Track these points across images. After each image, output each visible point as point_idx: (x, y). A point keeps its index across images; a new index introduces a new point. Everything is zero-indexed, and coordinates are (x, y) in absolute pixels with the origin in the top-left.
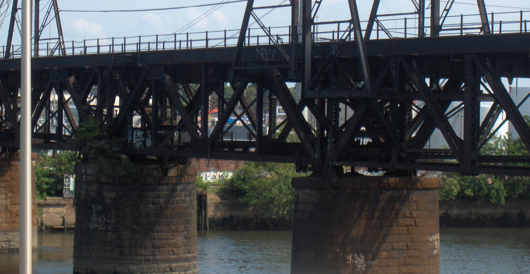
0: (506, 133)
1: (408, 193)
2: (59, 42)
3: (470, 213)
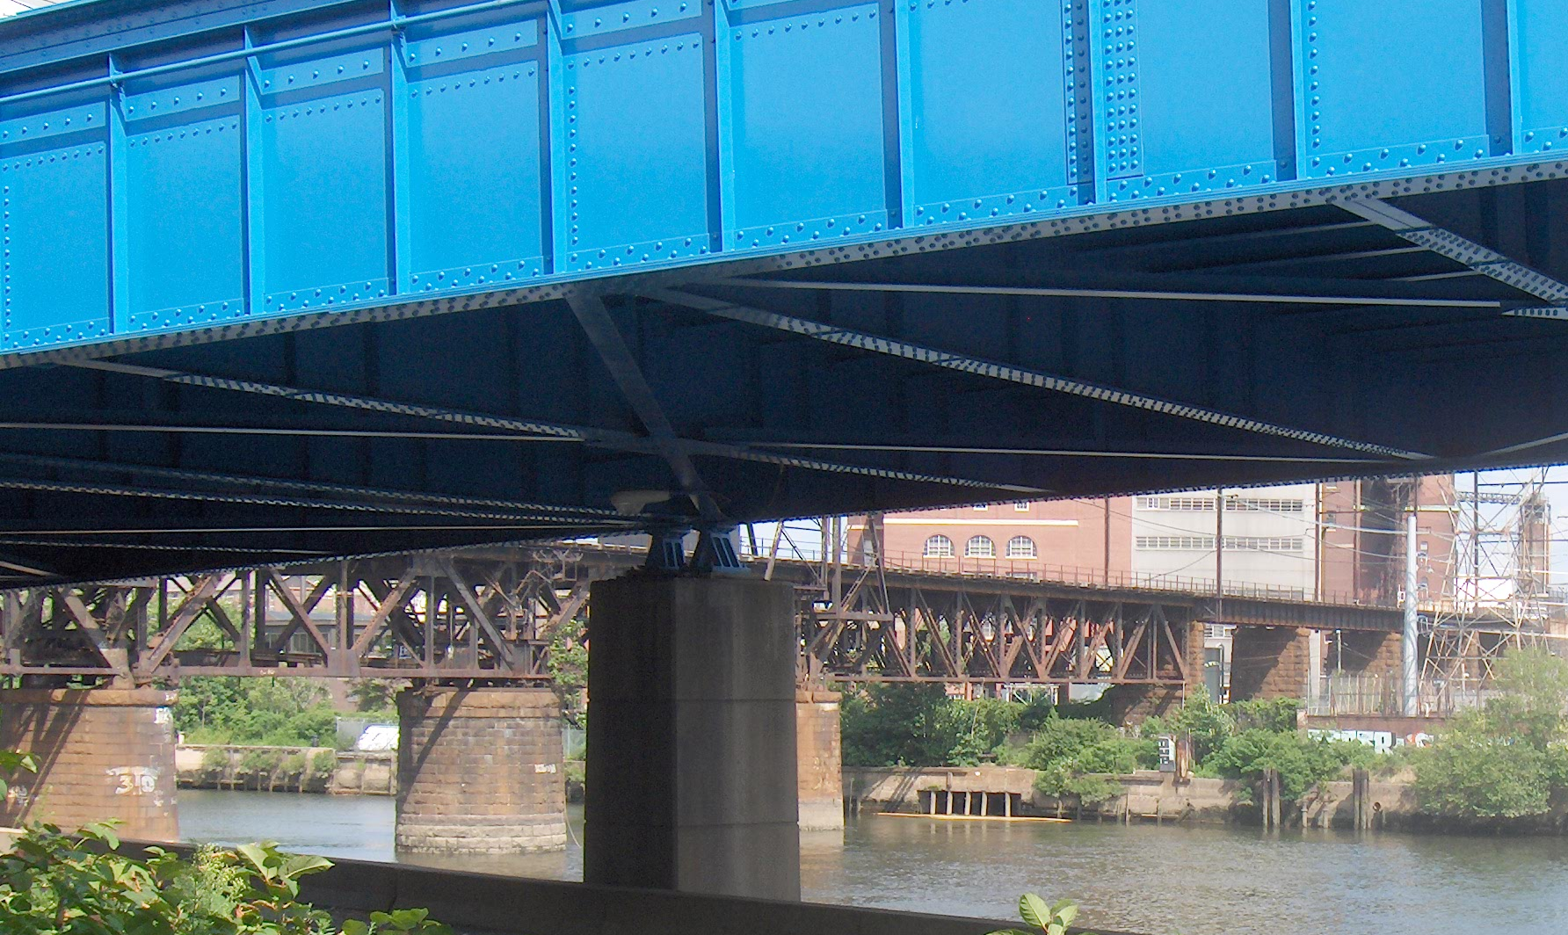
1: (81, 710)
2: (429, 727)
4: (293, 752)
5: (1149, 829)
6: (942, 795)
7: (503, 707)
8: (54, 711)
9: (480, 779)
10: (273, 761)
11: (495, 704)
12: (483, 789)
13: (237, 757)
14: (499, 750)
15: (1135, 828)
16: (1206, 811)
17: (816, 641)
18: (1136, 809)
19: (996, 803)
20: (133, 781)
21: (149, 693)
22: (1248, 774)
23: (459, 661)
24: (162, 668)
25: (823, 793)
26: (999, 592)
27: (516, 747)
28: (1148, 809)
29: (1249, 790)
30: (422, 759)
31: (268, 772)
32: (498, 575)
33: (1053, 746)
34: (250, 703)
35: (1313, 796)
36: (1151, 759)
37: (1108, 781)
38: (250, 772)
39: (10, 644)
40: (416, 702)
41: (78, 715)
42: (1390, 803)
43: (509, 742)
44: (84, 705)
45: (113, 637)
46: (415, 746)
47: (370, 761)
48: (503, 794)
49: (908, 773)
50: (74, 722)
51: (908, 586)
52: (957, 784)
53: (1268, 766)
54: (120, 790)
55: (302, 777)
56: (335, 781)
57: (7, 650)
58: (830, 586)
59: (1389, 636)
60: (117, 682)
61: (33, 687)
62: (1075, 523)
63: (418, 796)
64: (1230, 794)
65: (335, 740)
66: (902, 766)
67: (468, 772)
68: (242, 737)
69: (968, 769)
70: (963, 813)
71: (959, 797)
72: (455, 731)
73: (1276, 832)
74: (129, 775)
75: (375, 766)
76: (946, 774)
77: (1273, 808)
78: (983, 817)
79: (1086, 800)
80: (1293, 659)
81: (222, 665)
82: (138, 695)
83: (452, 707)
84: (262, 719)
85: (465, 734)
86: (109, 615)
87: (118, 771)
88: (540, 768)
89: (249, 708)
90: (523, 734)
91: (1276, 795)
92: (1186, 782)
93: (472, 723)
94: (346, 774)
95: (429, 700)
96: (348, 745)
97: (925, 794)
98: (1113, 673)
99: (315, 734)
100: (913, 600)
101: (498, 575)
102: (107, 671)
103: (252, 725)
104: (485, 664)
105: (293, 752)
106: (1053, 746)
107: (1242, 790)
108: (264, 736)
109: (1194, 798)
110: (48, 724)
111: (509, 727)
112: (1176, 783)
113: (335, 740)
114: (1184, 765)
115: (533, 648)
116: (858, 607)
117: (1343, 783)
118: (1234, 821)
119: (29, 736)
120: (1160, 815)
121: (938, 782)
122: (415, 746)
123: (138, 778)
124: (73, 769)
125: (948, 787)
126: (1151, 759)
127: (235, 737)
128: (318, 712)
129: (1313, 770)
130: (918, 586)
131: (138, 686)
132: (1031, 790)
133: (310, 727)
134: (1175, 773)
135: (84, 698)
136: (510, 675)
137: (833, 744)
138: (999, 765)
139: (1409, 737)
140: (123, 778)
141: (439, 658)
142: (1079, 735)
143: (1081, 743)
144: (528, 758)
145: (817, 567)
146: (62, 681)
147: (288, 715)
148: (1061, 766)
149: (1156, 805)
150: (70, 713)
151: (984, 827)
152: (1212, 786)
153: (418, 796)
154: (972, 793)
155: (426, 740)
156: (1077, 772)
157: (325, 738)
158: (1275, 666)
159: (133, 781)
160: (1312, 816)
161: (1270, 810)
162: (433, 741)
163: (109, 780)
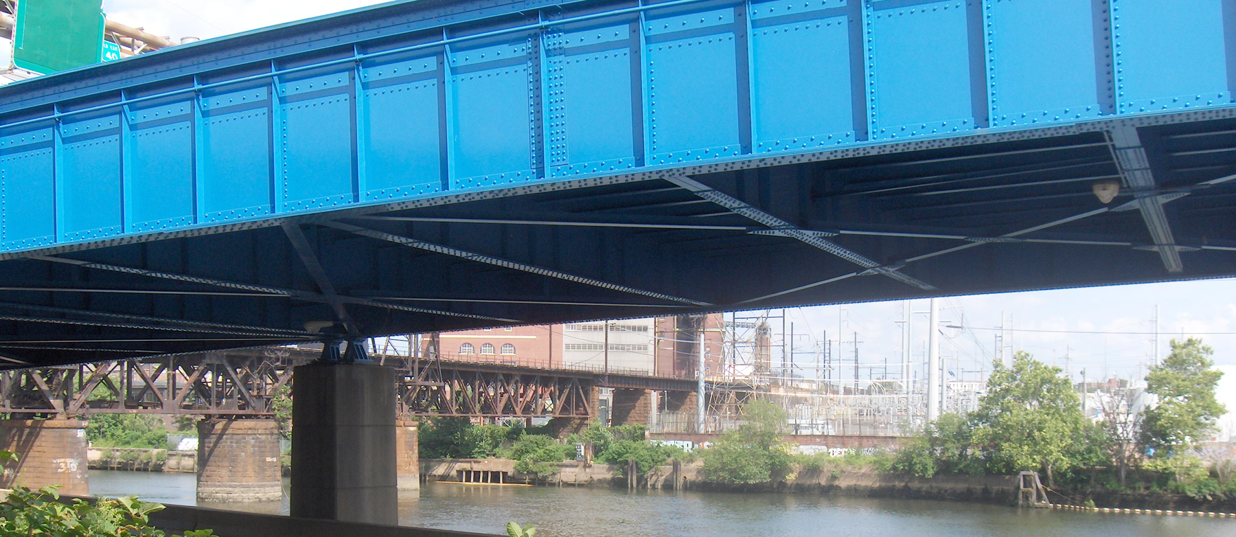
0: (1222, 374)
1: (40, 430)
2: (213, 439)
3: (931, 486)
4: (146, 451)
5: (571, 489)
6: (468, 473)
7: (250, 429)
8: (27, 431)
9: (239, 465)
10: (136, 456)
11: (246, 427)
12: (240, 469)
13: (118, 453)
14: (248, 450)
15: (564, 489)
16: (600, 481)
17: (406, 396)
18: (565, 480)
19: (495, 477)
20: (66, 465)
21: (74, 422)
22: (620, 462)
23: (228, 406)
24: (80, 409)
25: (409, 472)
26: (497, 372)
27: (256, 449)
28: (571, 479)
29: (621, 470)
30: (210, 455)
31: (133, 461)
32: (248, 363)
33: (524, 448)
34: (124, 427)
35: (653, 473)
36: (572, 455)
37: (551, 466)
38: (125, 461)
39: (5, 398)
40: (207, 426)
41: (39, 433)
42: (691, 476)
43: (253, 446)
44: (42, 428)
45: (56, 394)
46: (206, 448)
47: (184, 456)
48: (250, 472)
49: (451, 461)
50: (37, 436)
51: (451, 369)
52: (476, 467)
53: (631, 458)
54: (60, 470)
55: (150, 464)
56: (167, 466)
57: (4, 401)
58: (413, 368)
59: (691, 394)
60: (58, 416)
61: (17, 419)
62: (535, 337)
63: (208, 473)
64: (611, 472)
65: (167, 445)
66: (448, 458)
67: (233, 461)
68: (121, 443)
69: (482, 460)
70: (479, 481)
71: (477, 473)
72: (226, 440)
73: (635, 491)
74: (64, 462)
75: (186, 458)
76: (470, 462)
77: (633, 479)
78: (489, 483)
79: (540, 475)
80: (643, 405)
81: (111, 408)
82: (68, 423)
83: (225, 429)
84: (130, 435)
85: (231, 442)
86: (54, 383)
87: (59, 461)
88: (269, 459)
89: (124, 429)
90: (260, 442)
91: (635, 472)
92: (590, 466)
93: (235, 437)
94: (172, 462)
95: (213, 426)
96: (173, 447)
97: (460, 472)
98: (535, 411)
99: (157, 442)
100: (454, 375)
101: (248, 363)
102: (53, 411)
103: (125, 438)
104: (241, 407)
105: (146, 451)
106: (524, 448)
107: (618, 470)
108: (131, 443)
109: (594, 474)
110: (24, 437)
111: (253, 439)
112: (585, 467)
113: (167, 445)
114: (589, 458)
115: (265, 400)
116: (427, 379)
117: (668, 467)
118: (614, 485)
119: (15, 443)
120: (577, 483)
121: (467, 466)
122: (206, 448)
123: (68, 464)
124: (36, 459)
125: (472, 468)
126: (572, 455)
127: (117, 444)
128: (158, 431)
129: (653, 460)
130: (456, 368)
131: (69, 418)
132: (513, 470)
133: (154, 439)
134: (584, 462)
135: (42, 424)
136: (254, 413)
137: (414, 447)
138: (497, 457)
139: (701, 444)
140: (61, 464)
141: (218, 404)
142: (536, 443)
143: (538, 447)
144: (262, 454)
145: (406, 359)
146: (31, 416)
147: (143, 433)
148: (528, 458)
149: (574, 478)
150: (35, 432)
151: (489, 489)
152: (603, 468)
153: (208, 473)
154: (483, 472)
155: (212, 445)
156: (535, 461)
157: (161, 444)
158: (634, 409)
159: (66, 465)
160: (652, 483)
161: (632, 480)
162: (215, 445)
163: (54, 465)
